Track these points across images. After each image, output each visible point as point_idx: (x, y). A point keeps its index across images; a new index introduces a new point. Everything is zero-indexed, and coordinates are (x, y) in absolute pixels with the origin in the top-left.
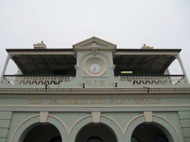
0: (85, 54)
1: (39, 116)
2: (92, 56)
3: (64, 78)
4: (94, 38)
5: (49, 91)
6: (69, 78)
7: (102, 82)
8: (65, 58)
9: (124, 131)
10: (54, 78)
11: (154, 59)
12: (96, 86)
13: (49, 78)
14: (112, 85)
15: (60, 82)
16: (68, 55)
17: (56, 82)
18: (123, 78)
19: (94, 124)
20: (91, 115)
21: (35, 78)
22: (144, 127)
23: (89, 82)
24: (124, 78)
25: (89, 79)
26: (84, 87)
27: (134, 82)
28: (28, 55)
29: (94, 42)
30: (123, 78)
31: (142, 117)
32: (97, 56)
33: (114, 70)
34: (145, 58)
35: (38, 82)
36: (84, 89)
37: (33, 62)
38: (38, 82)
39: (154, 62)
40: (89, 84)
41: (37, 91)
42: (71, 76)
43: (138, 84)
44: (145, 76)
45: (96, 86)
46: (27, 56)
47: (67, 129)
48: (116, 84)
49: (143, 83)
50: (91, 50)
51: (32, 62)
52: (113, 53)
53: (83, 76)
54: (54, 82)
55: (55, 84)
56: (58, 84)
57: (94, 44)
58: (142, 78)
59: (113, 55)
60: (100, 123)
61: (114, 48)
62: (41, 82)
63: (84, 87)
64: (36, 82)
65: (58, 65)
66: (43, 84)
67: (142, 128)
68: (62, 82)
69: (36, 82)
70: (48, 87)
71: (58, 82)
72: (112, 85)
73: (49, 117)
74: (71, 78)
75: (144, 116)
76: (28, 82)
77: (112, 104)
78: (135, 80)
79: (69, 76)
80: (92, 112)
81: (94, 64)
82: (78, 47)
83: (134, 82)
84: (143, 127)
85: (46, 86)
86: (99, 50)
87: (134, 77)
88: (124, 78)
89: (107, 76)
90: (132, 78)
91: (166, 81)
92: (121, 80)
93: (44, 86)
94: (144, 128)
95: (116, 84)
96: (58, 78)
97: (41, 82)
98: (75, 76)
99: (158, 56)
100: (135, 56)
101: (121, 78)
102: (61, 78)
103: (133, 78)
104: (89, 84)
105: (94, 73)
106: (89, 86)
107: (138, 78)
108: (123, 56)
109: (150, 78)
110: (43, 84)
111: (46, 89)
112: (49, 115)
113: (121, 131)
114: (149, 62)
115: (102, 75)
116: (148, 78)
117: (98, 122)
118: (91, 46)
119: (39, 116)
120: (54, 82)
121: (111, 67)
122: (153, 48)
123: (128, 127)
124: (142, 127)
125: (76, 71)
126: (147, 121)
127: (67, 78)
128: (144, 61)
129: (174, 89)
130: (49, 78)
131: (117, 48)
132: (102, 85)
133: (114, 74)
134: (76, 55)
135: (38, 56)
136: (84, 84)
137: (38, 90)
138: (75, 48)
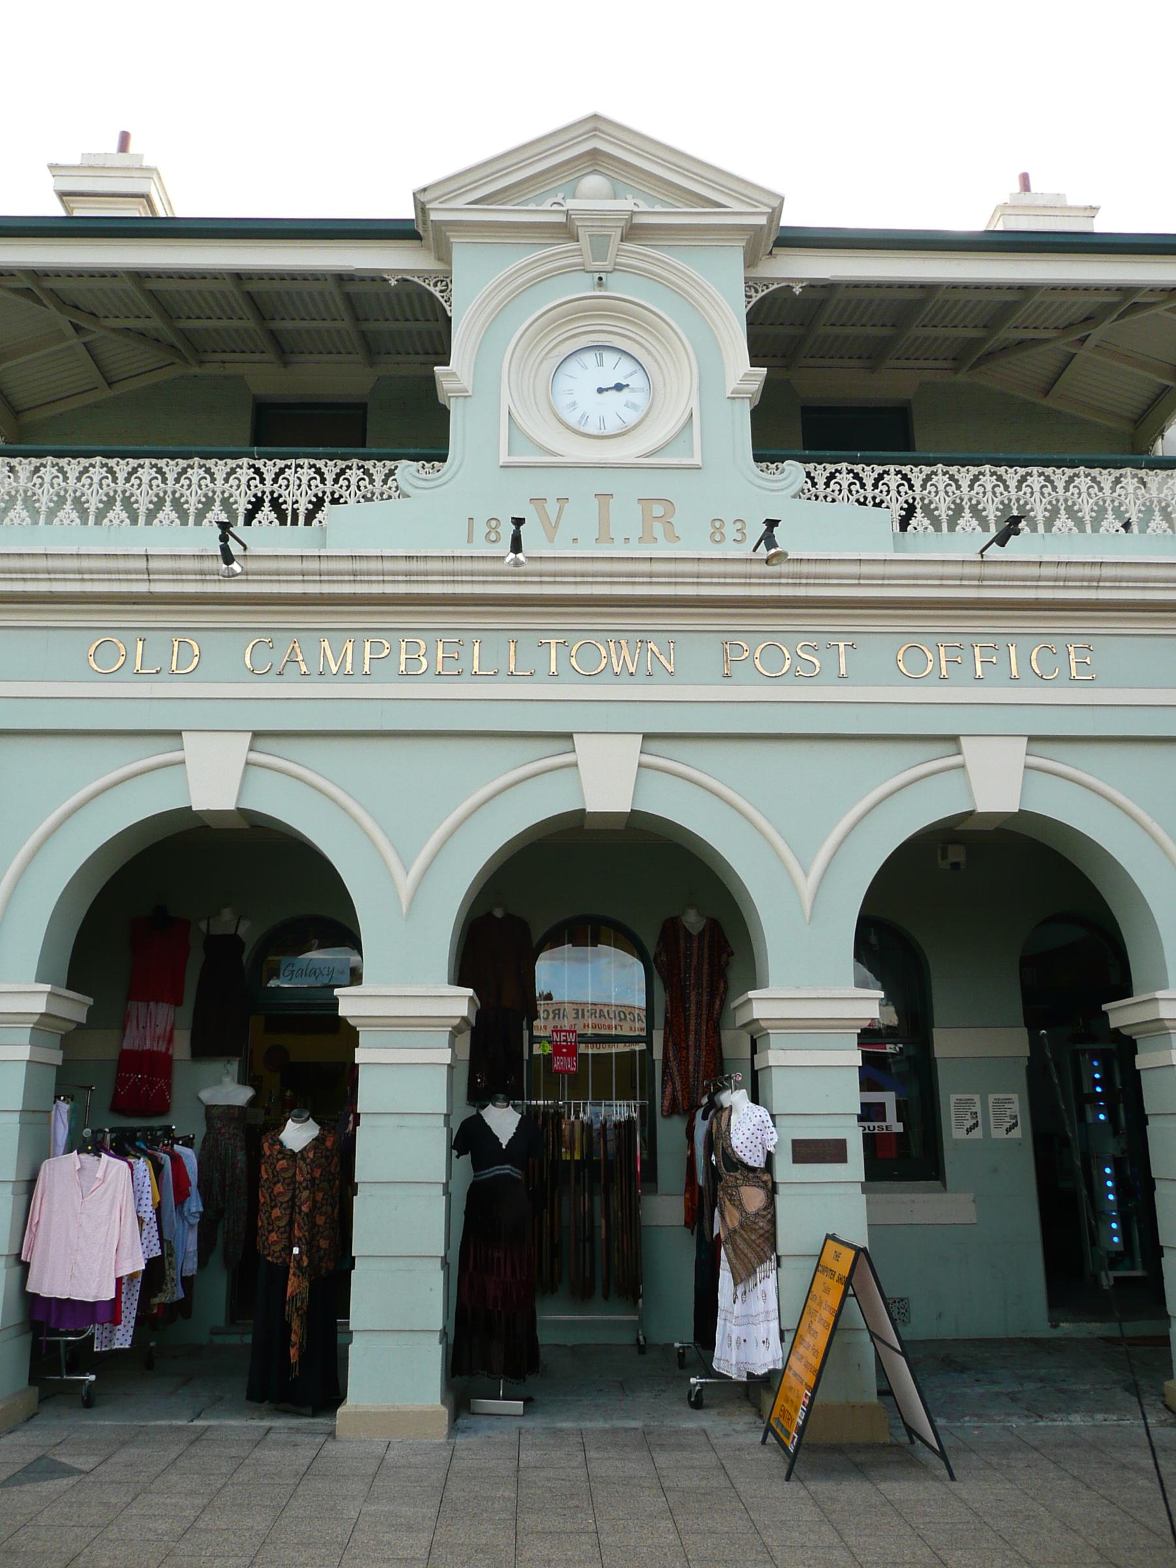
0: (519, 272)
1: (183, 762)
2: (580, 287)
3: (354, 475)
4: (595, 123)
5: (245, 572)
6: (391, 473)
7: (658, 510)
8: (348, 297)
9: (806, 874)
10: (269, 468)
11: (1090, 319)
12: (647, 538)
13: (86, 470)
14: (730, 531)
15: (318, 504)
16: (376, 278)
17: (288, 507)
18: (821, 481)
19: (587, 827)
20: (955, 760)
21: (269, 472)
22: (957, 854)
23: (552, 508)
24: (832, 476)
25: (550, 486)
26: (516, 546)
27: (910, 510)
28: (37, 274)
29: (594, 159)
30: (821, 481)
31: (954, 777)
32: (619, 287)
33: (755, 413)
34: (823, 303)
35: (143, 506)
36: (517, 563)
37: (77, 328)
38: (143, 506)
39: (1083, 340)
40: (551, 529)
41: (148, 572)
42: (794, 458)
43: (938, 528)
44: (949, 463)
45: (604, 537)
46: (27, 284)
47: (797, 872)
48: (772, 524)
49: (273, 515)
50: (566, 230)
51: (70, 331)
52: (751, 261)
53: (504, 458)
54: (276, 504)
55: (283, 522)
56: (308, 521)
57: (593, 182)
58: (976, 479)
59: (751, 284)
60: (634, 815)
61: (762, 220)
62: (168, 507)
63: (516, 546)
64: (128, 504)
65: (286, 364)
66: (184, 523)
67: (944, 865)
68: (335, 501)
69: (128, 504)
70: (235, 548)
71: (303, 507)
72: (730, 531)
73: (252, 769)
74: (406, 469)
75: (963, 766)
76: (61, 501)
77: (727, 676)
78: (268, 487)
79: (395, 458)
80: (183, 733)
81: (590, 358)
82: (460, 203)
83: (910, 510)
84: (952, 859)
85: (224, 538)
86: (634, 231)
87: (906, 469)
88: (832, 476)
89: (697, 460)
90: (893, 480)
91: (1164, 510)
92: (809, 491)
93: (207, 539)
94: (955, 866)
95: (772, 524)
96: (306, 473)
97: (168, 507)
98: (443, 459)
99: (1126, 291)
100: (928, 289)
101: (808, 474)
102: (330, 468)
103: (905, 477)
104: (551, 529)
105: (568, 427)
106: (551, 540)
107: (941, 480)
108: (829, 288)
109: (1083, 482)
110: (184, 523)
111: (228, 557)
112: (255, 757)
113: (390, 874)
114: (1045, 341)
115: (646, 456)
116: (1117, 481)
117: (229, 805)
118: (570, 204)
119: (183, 762)
120: (276, 504)
121: (732, 384)
122: (1093, 210)
123: (841, 843)
124: (944, 857)
125: (444, 413)
126: (594, 805)
127: (378, 469)
128: (1007, 334)
129: (141, 564)
130: (86, 470)
131: (788, 219)
132: (658, 529)
133: (756, 445)
134: (445, 279)
135: (362, 279)
136: (518, 522)
137: (154, 564)
138: (434, 216)
